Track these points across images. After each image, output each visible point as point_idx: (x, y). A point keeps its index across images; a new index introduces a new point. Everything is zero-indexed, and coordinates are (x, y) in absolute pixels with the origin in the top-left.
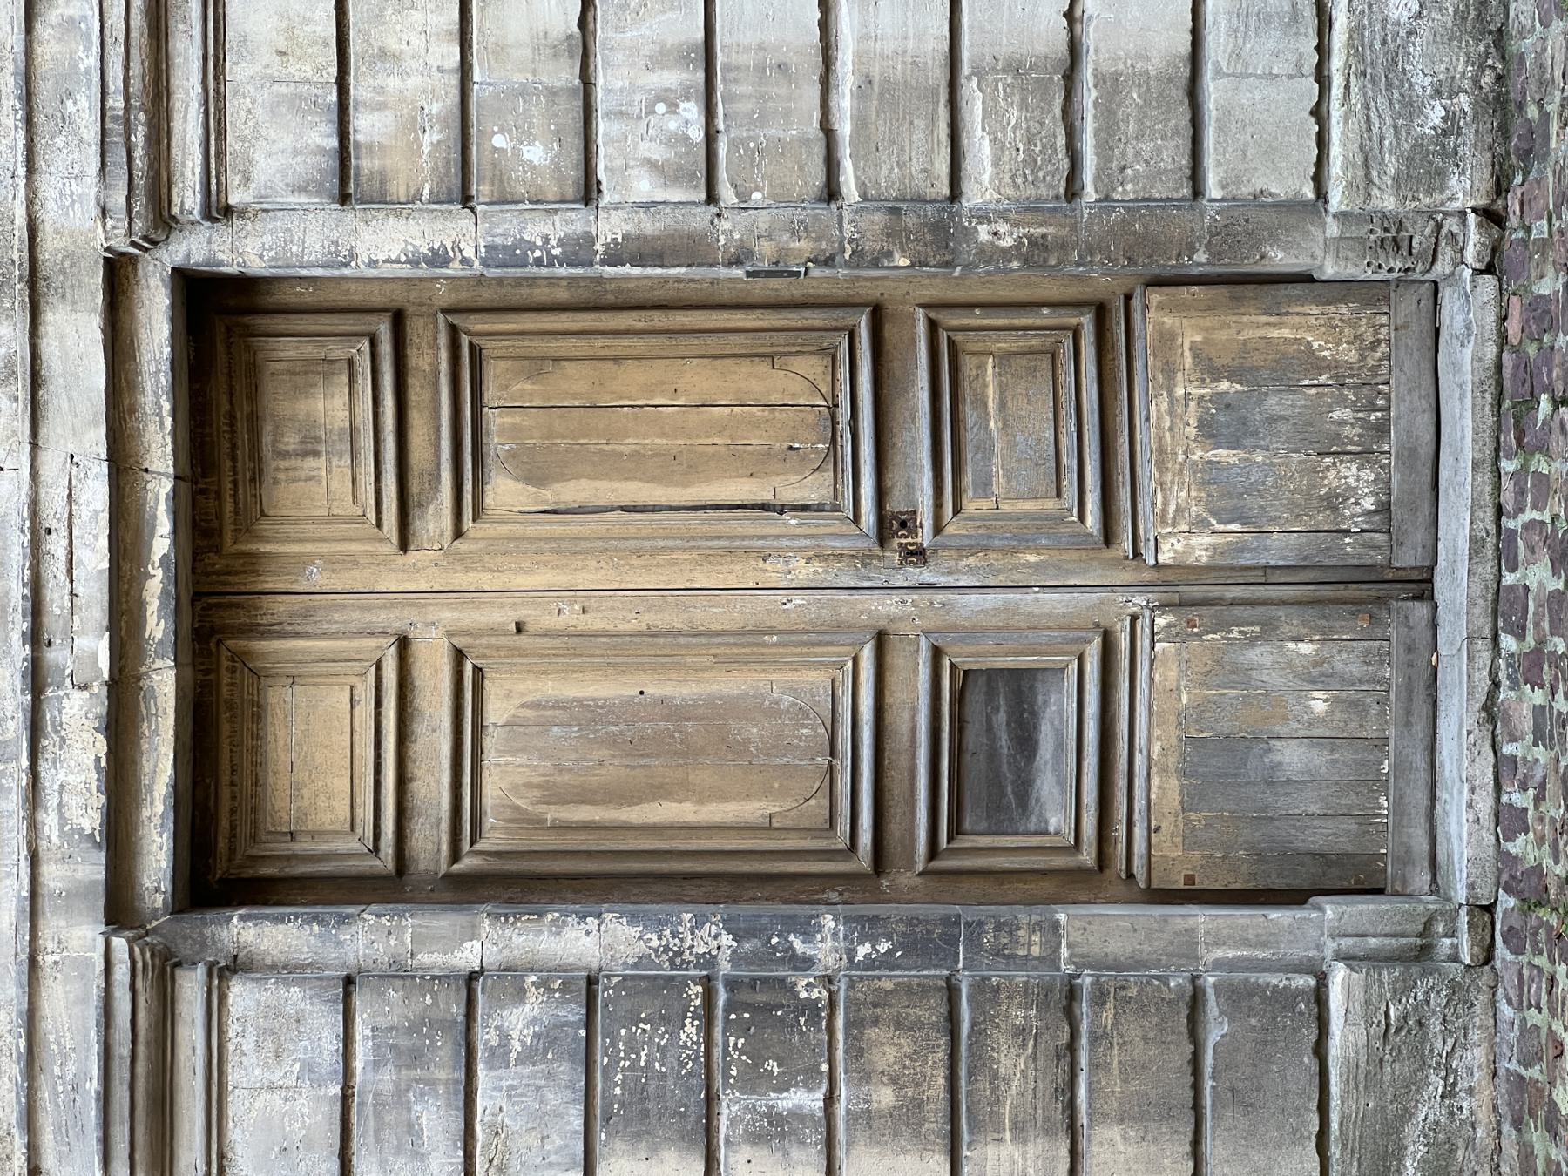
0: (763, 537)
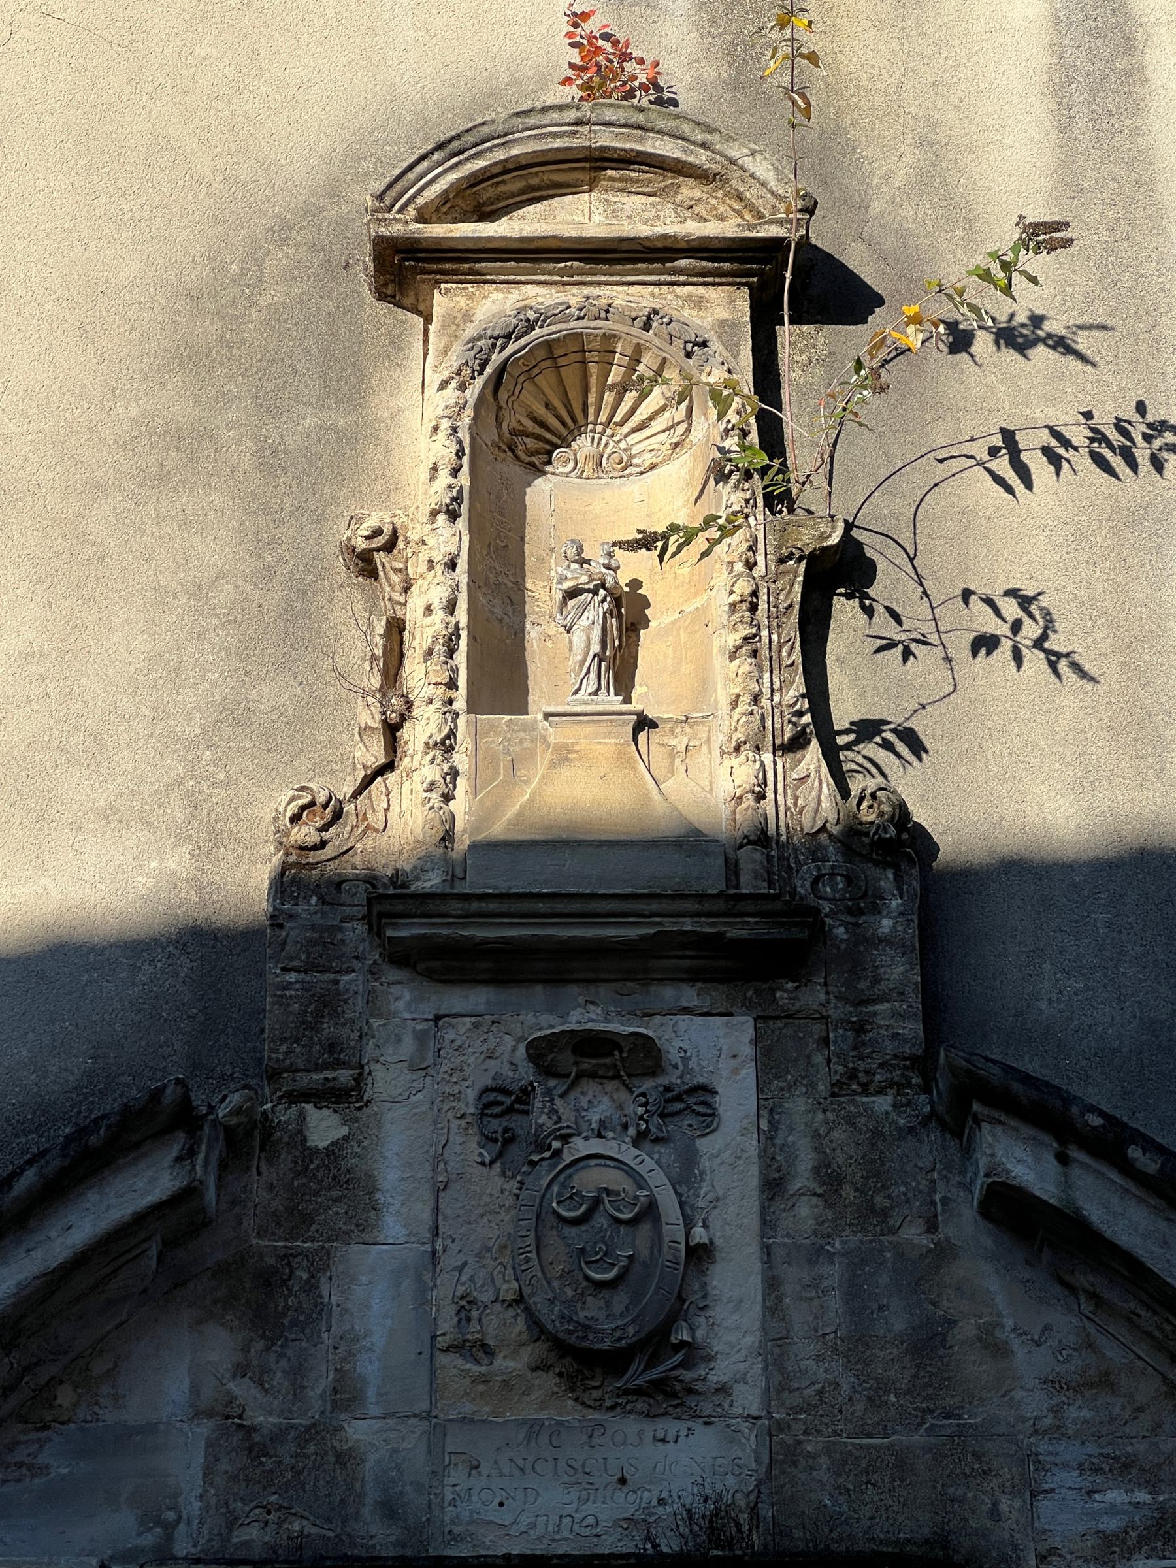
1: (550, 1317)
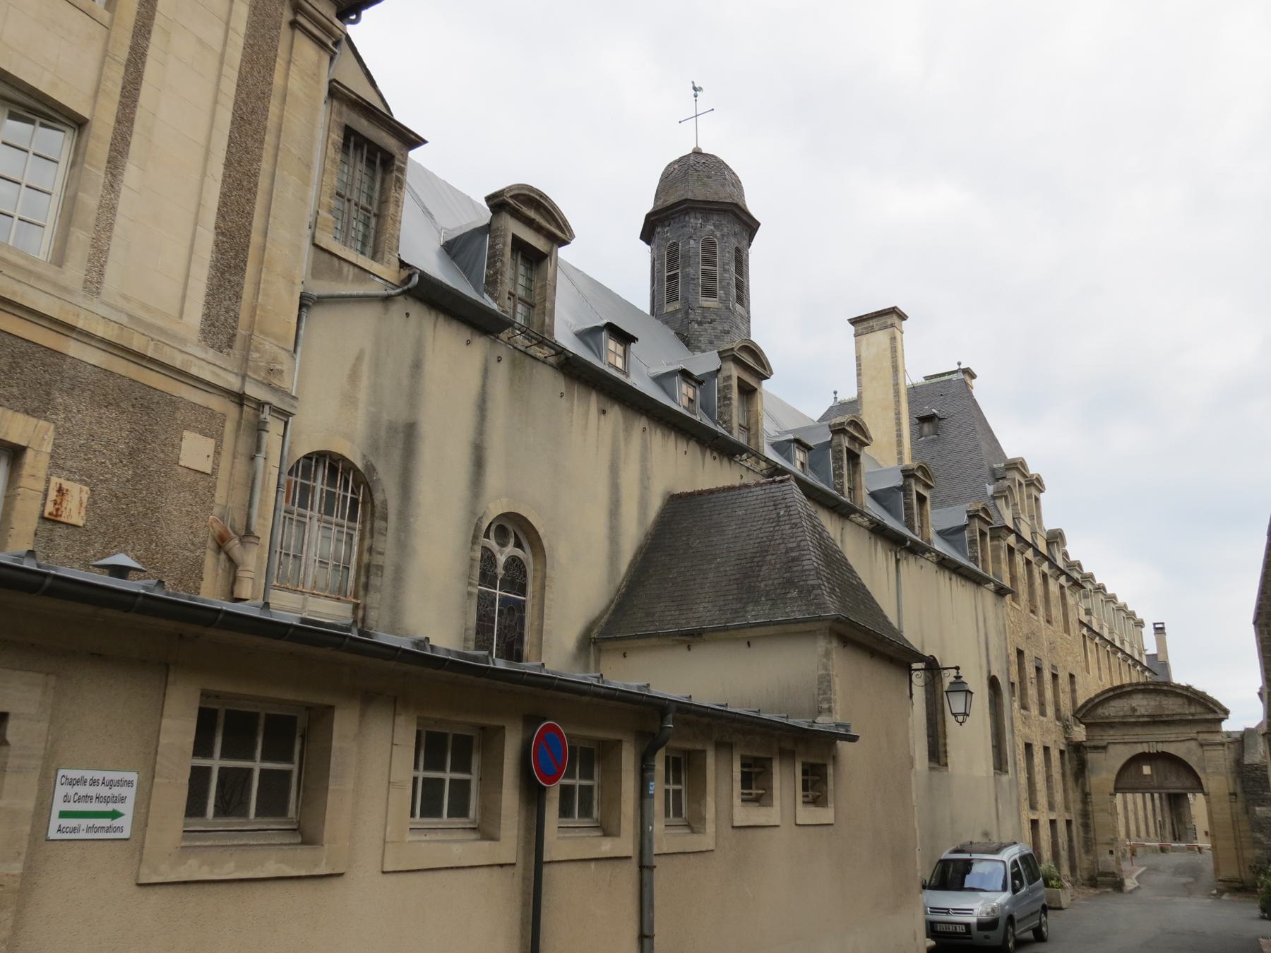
0: (94, 782)
1: (230, 505)
